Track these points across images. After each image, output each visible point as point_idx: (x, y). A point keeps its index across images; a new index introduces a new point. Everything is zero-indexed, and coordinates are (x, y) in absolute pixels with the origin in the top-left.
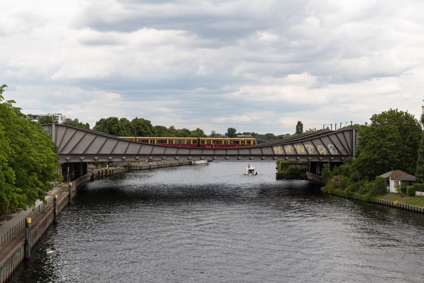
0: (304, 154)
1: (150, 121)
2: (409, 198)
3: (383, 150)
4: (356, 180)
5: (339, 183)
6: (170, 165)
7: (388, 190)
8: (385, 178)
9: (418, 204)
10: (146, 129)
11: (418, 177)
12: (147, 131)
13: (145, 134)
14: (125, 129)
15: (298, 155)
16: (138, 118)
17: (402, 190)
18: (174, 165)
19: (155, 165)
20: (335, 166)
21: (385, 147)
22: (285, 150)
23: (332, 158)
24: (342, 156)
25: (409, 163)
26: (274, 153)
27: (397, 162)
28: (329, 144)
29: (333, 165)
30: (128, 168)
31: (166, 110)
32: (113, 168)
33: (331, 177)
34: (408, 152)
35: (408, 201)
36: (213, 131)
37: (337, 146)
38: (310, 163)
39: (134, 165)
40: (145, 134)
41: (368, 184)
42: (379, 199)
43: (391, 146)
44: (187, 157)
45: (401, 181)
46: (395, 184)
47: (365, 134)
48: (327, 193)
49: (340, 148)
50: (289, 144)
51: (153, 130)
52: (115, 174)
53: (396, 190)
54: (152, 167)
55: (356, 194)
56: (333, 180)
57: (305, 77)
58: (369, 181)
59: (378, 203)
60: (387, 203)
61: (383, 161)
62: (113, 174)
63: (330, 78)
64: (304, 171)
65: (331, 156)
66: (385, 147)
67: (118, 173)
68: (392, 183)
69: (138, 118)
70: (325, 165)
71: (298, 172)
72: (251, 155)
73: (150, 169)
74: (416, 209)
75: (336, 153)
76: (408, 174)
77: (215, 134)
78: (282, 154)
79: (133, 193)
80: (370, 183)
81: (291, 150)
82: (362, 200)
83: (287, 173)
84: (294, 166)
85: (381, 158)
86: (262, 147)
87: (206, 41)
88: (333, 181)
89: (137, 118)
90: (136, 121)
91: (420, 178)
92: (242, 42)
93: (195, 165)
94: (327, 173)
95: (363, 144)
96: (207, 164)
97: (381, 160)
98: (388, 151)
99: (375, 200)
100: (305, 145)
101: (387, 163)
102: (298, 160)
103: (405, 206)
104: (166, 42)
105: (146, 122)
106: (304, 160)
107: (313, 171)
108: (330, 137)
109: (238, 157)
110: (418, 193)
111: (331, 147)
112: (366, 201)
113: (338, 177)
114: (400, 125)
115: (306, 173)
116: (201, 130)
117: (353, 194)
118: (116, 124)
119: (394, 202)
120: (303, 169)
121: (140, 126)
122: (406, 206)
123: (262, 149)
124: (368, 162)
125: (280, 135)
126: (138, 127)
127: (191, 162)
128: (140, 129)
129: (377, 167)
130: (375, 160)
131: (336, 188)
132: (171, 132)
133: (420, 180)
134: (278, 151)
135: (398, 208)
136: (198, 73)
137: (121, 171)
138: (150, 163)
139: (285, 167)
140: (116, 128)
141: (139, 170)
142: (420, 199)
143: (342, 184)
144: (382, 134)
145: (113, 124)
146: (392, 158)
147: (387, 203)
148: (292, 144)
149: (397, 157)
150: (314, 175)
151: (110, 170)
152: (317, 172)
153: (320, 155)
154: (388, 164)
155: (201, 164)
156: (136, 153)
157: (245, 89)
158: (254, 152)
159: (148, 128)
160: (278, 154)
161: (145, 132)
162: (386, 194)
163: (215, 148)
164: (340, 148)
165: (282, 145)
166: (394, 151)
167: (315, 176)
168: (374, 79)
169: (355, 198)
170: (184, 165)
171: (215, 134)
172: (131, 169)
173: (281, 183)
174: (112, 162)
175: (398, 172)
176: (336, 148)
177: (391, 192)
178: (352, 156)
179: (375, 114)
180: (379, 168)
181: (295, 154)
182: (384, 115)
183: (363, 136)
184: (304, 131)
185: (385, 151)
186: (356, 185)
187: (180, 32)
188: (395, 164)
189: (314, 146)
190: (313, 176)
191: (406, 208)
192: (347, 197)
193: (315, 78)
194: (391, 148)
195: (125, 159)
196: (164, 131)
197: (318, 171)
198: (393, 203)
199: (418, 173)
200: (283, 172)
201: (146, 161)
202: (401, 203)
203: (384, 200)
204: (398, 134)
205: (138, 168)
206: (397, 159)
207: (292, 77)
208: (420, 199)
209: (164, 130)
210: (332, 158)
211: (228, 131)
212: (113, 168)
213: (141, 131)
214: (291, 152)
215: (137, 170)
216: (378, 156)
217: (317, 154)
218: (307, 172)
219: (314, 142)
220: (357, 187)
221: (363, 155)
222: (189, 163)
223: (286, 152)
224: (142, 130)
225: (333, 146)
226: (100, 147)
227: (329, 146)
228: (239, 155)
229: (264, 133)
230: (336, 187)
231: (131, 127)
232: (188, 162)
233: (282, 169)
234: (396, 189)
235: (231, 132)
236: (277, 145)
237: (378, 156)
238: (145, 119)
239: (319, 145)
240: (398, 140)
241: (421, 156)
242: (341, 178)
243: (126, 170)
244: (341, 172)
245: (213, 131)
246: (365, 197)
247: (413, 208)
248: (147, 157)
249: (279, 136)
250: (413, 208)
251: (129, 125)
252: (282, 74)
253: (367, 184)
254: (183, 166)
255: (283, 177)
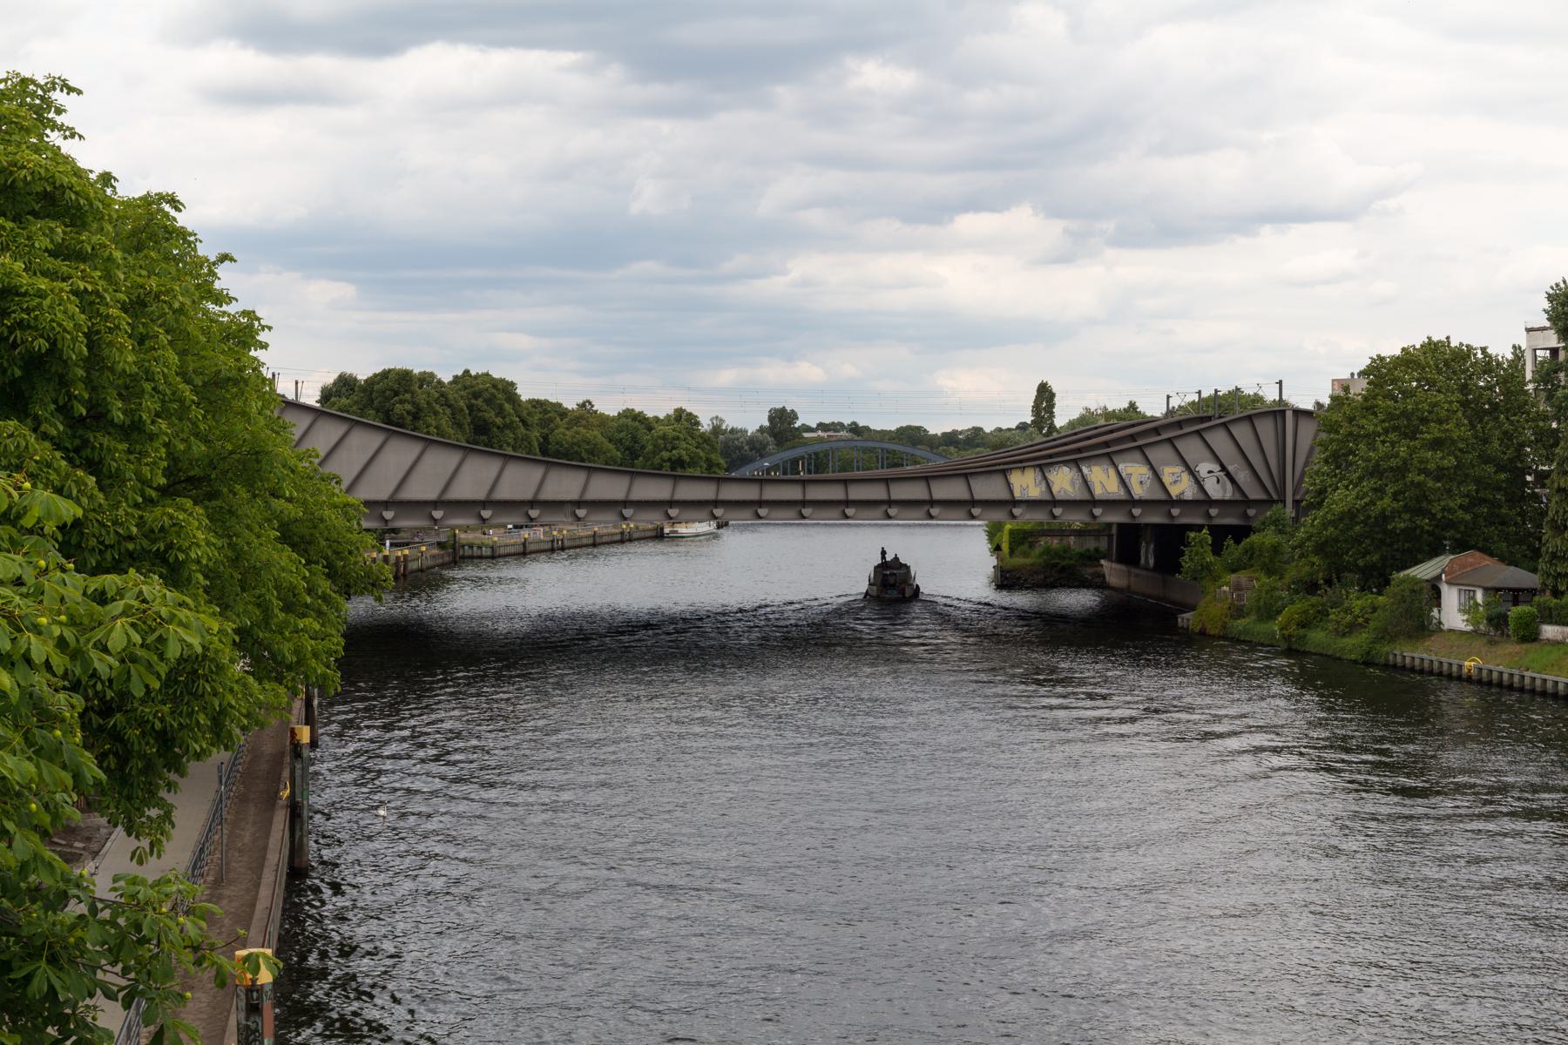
0: (1117, 498)
1: (512, 384)
2: (1518, 648)
3: (1412, 482)
4: (1311, 587)
5: (1248, 599)
6: (590, 541)
7: (1435, 621)
8: (1427, 581)
9: (1556, 668)
10: (500, 412)
11: (1549, 575)
12: (504, 418)
13: (498, 428)
14: (438, 412)
15: (1094, 502)
16: (473, 373)
17: (1490, 620)
18: (605, 539)
19: (541, 541)
20: (1230, 541)
21: (1419, 469)
22: (1051, 484)
23: (1213, 512)
24: (1248, 502)
25: (1500, 528)
26: (1012, 492)
27: (1461, 522)
28: (1203, 461)
29: (1220, 534)
30: (450, 550)
31: (523, 341)
32: (406, 552)
33: (1216, 579)
34: (1499, 489)
35: (1516, 659)
36: (717, 417)
37: (1230, 468)
38: (1114, 531)
39: (472, 541)
40: (498, 428)
41: (1359, 602)
42: (1405, 654)
43: (1440, 469)
44: (619, 509)
45: (1486, 589)
46: (1463, 601)
47: (1345, 424)
48: (1203, 633)
49: (1243, 476)
50: (1065, 463)
51: (524, 414)
52: (413, 572)
53: (1467, 620)
54: (531, 547)
55: (1318, 638)
56: (1225, 588)
57: (1022, 220)
58: (1362, 589)
59: (1404, 667)
60: (1436, 665)
61: (1410, 520)
62: (407, 572)
63: (1109, 226)
64: (1093, 558)
65: (1210, 502)
66: (1421, 471)
67: (422, 571)
68: (1451, 597)
69: (473, 373)
70: (1192, 535)
71: (1072, 562)
72: (932, 503)
73: (524, 553)
74: (1549, 685)
75: (1228, 493)
76: (1503, 567)
77: (724, 427)
78: (1039, 498)
79: (527, 636)
80: (1370, 599)
81: (1073, 484)
82: (1340, 659)
83: (1032, 565)
84: (1055, 541)
85: (1406, 508)
86: (972, 474)
87: (658, 91)
88: (1225, 592)
89: (467, 372)
90: (465, 381)
91: (1556, 578)
92: (786, 94)
93: (676, 538)
94: (1202, 565)
95: (1338, 459)
96: (715, 536)
97: (1406, 516)
98: (1430, 484)
99: (1391, 657)
100: (1121, 467)
101: (1427, 528)
102: (1054, 517)
103: (1505, 677)
104: (513, 97)
105: (500, 387)
106: (1077, 519)
107: (1127, 556)
108: (1208, 437)
109: (843, 508)
110: (1550, 631)
111: (1210, 472)
112: (1355, 662)
113: (1242, 577)
114: (1464, 389)
115: (1102, 566)
116: (690, 414)
117: (1305, 636)
118: (406, 391)
119: (1466, 663)
120: (1088, 550)
121: (479, 402)
122: (1512, 675)
123: (972, 482)
124: (1357, 523)
125: (949, 430)
126: (472, 405)
127: (662, 529)
128: (479, 410)
129: (1388, 541)
130: (1384, 518)
131: (1239, 617)
132: (584, 422)
133: (1555, 587)
134: (1025, 486)
135: (1480, 682)
136: (635, 208)
137: (430, 563)
138: (525, 533)
139: (1023, 544)
140: (408, 407)
141: (486, 557)
142: (1561, 652)
143: (1262, 603)
144: (1408, 425)
145: (396, 394)
146: (1443, 510)
147: (1436, 665)
148: (1076, 463)
149: (1461, 507)
150: (1135, 571)
151: (398, 558)
152: (1143, 561)
153: (1170, 502)
154: (1428, 531)
155: (698, 535)
156: (529, 496)
157: (805, 266)
158: (942, 491)
159: (507, 406)
160: (1026, 498)
161: (499, 421)
162: (1430, 636)
163: (807, 476)
164: (1243, 476)
165: (1040, 466)
166: (1447, 487)
167: (1137, 575)
168: (1267, 230)
169: (1313, 651)
170: (639, 539)
171: (724, 427)
172: (461, 553)
173: (1021, 600)
174: (395, 531)
175: (1472, 557)
176: (1228, 475)
177: (1446, 627)
178: (1284, 502)
179: (1379, 356)
180: (1395, 547)
181: (1086, 497)
182: (1408, 360)
183: (1337, 432)
184: (1060, 421)
185: (1419, 485)
186: (1313, 606)
187: (568, 58)
188: (1452, 531)
189: (1152, 468)
190: (1129, 573)
191: (1512, 684)
192: (1284, 646)
193: (1056, 227)
194: (1440, 474)
195: (394, 517)
196: (558, 419)
197: (1147, 558)
198: (1460, 667)
199: (1550, 562)
200: (1018, 561)
201: (510, 526)
202: (1491, 667)
203: (1425, 656)
204: (1464, 425)
205: (486, 552)
206: (1460, 513)
207: (969, 224)
208: (1561, 652)
209: (556, 415)
210: (1213, 512)
211: (771, 419)
212: (406, 552)
213: (485, 420)
214: (1070, 489)
215: (481, 557)
216: (1395, 505)
217: (1160, 496)
218: (1103, 562)
219: (1153, 454)
220: (1319, 612)
221: (1342, 499)
222: (654, 534)
223: (1055, 490)
224: (486, 415)
225: (1216, 468)
226: (400, 476)
227: (1205, 468)
228: (890, 503)
229: (892, 425)
230: (1239, 612)
231: (450, 406)
232: (650, 530)
233: (1012, 551)
234: (1466, 617)
235: (782, 420)
236: (1021, 464)
237: (1395, 505)
238: (496, 375)
239: (1168, 464)
240: (1461, 445)
241: (1561, 501)
242: (1254, 583)
243: (447, 559)
244: (1251, 558)
245: (717, 417)
246: (1353, 645)
247: (1538, 683)
248: (569, 509)
249: (944, 434)
250: (1538, 683)
251: (447, 398)
252: (938, 212)
253: (1358, 602)
254: (636, 543)
255: (1019, 578)
